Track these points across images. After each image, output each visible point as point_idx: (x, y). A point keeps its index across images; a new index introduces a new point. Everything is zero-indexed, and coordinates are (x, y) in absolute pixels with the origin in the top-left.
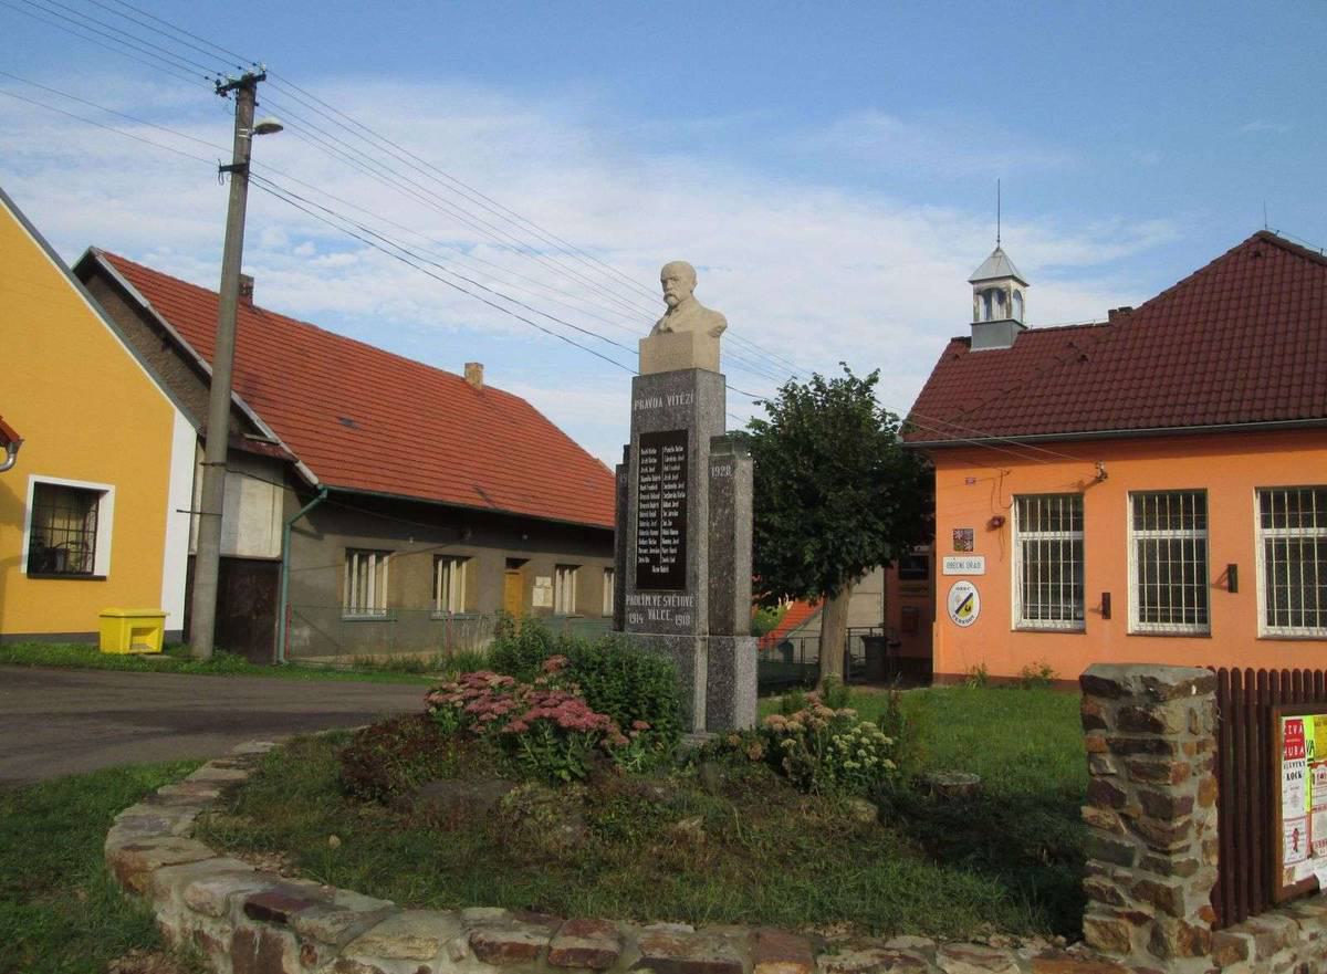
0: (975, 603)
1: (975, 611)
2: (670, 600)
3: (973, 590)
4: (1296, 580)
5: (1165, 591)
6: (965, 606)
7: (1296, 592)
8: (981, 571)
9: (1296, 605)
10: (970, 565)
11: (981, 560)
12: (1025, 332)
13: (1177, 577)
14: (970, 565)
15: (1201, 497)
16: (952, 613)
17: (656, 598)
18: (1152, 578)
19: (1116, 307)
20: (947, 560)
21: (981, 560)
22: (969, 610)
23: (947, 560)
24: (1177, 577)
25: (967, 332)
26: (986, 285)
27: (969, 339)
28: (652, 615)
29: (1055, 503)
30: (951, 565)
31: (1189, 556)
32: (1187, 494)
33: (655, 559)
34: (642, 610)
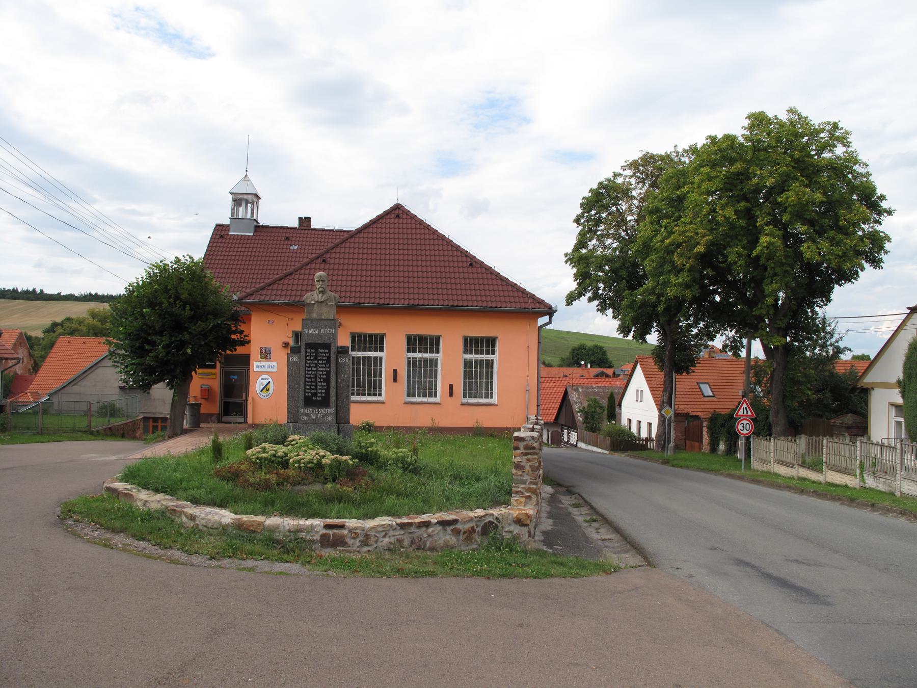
0: (271, 386)
1: (271, 391)
2: (322, 411)
3: (270, 380)
4: (420, 377)
5: (358, 381)
6: (266, 388)
7: (420, 382)
8: (275, 370)
9: (419, 388)
10: (269, 367)
11: (275, 364)
12: (258, 228)
13: (369, 375)
14: (269, 367)
15: (382, 337)
16: (258, 391)
17: (316, 410)
18: (375, 382)
19: (303, 216)
20: (256, 364)
21: (275, 364)
22: (268, 390)
23: (256, 364)
24: (369, 375)
25: (227, 222)
26: (240, 196)
27: (227, 226)
28: (313, 417)
29: (476, 393)
30: (259, 367)
31: (370, 365)
32: (376, 336)
33: (314, 394)
34: (307, 414)
